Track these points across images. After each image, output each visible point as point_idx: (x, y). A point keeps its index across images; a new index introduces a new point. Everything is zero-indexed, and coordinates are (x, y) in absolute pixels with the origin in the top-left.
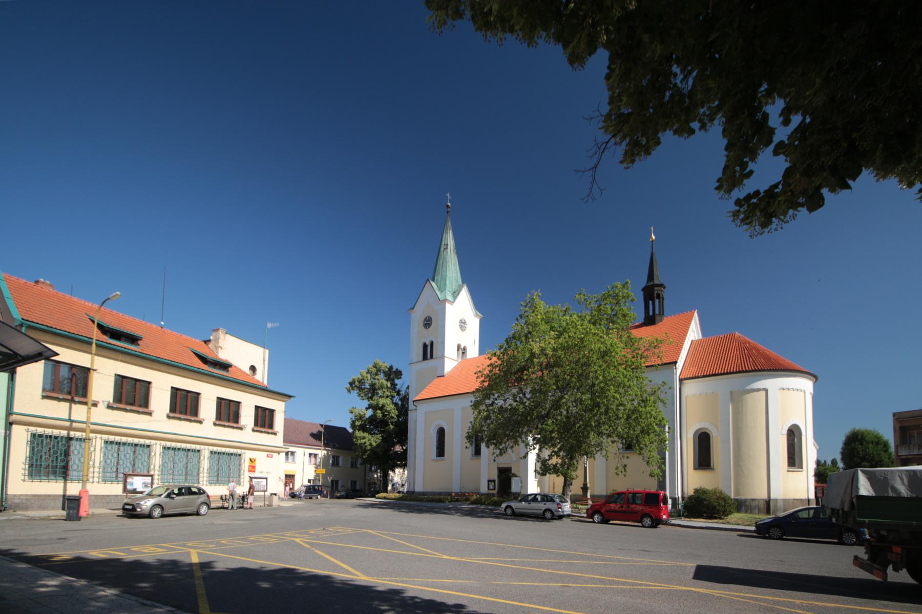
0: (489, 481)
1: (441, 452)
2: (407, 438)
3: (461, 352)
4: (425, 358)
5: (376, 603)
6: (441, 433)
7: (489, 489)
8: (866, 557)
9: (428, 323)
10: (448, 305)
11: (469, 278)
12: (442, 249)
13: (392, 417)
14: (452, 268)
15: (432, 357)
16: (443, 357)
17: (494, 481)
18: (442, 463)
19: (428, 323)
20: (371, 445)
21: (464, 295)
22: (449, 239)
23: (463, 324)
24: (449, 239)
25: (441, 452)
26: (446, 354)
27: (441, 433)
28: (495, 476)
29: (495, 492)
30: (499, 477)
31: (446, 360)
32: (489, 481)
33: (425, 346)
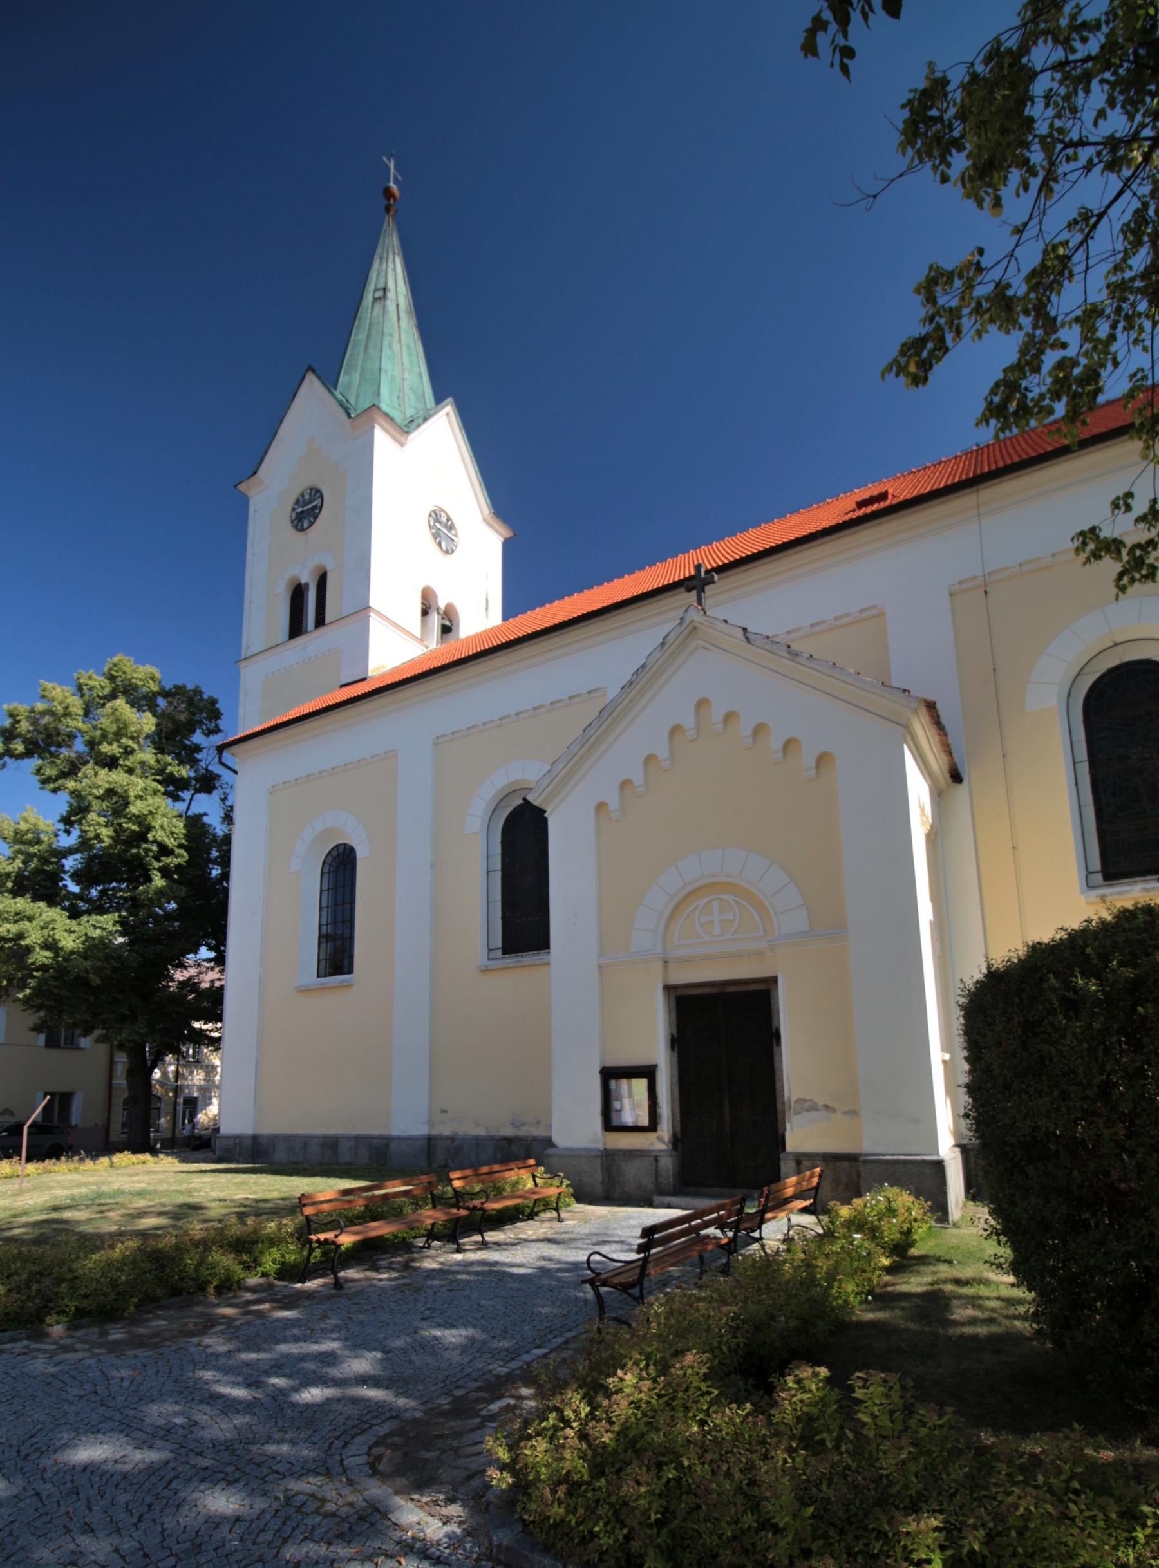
0: (609, 1075)
1: (337, 955)
2: (351, 957)
3: (435, 621)
4: (296, 628)
5: (208, 1375)
6: (341, 866)
7: (609, 1125)
8: (22, 943)
9: (307, 511)
10: (382, 439)
11: (454, 376)
12: (368, 298)
13: (164, 851)
14: (393, 346)
15: (320, 622)
16: (364, 609)
17: (648, 1073)
18: (520, 977)
19: (307, 511)
20: (50, 945)
21: (443, 432)
22: (392, 276)
23: (442, 528)
24: (392, 276)
25: (337, 955)
26: (373, 603)
27: (341, 866)
28: (652, 1041)
29: (660, 1141)
30: (676, 1043)
31: (374, 623)
32: (609, 1075)
33: (298, 593)
